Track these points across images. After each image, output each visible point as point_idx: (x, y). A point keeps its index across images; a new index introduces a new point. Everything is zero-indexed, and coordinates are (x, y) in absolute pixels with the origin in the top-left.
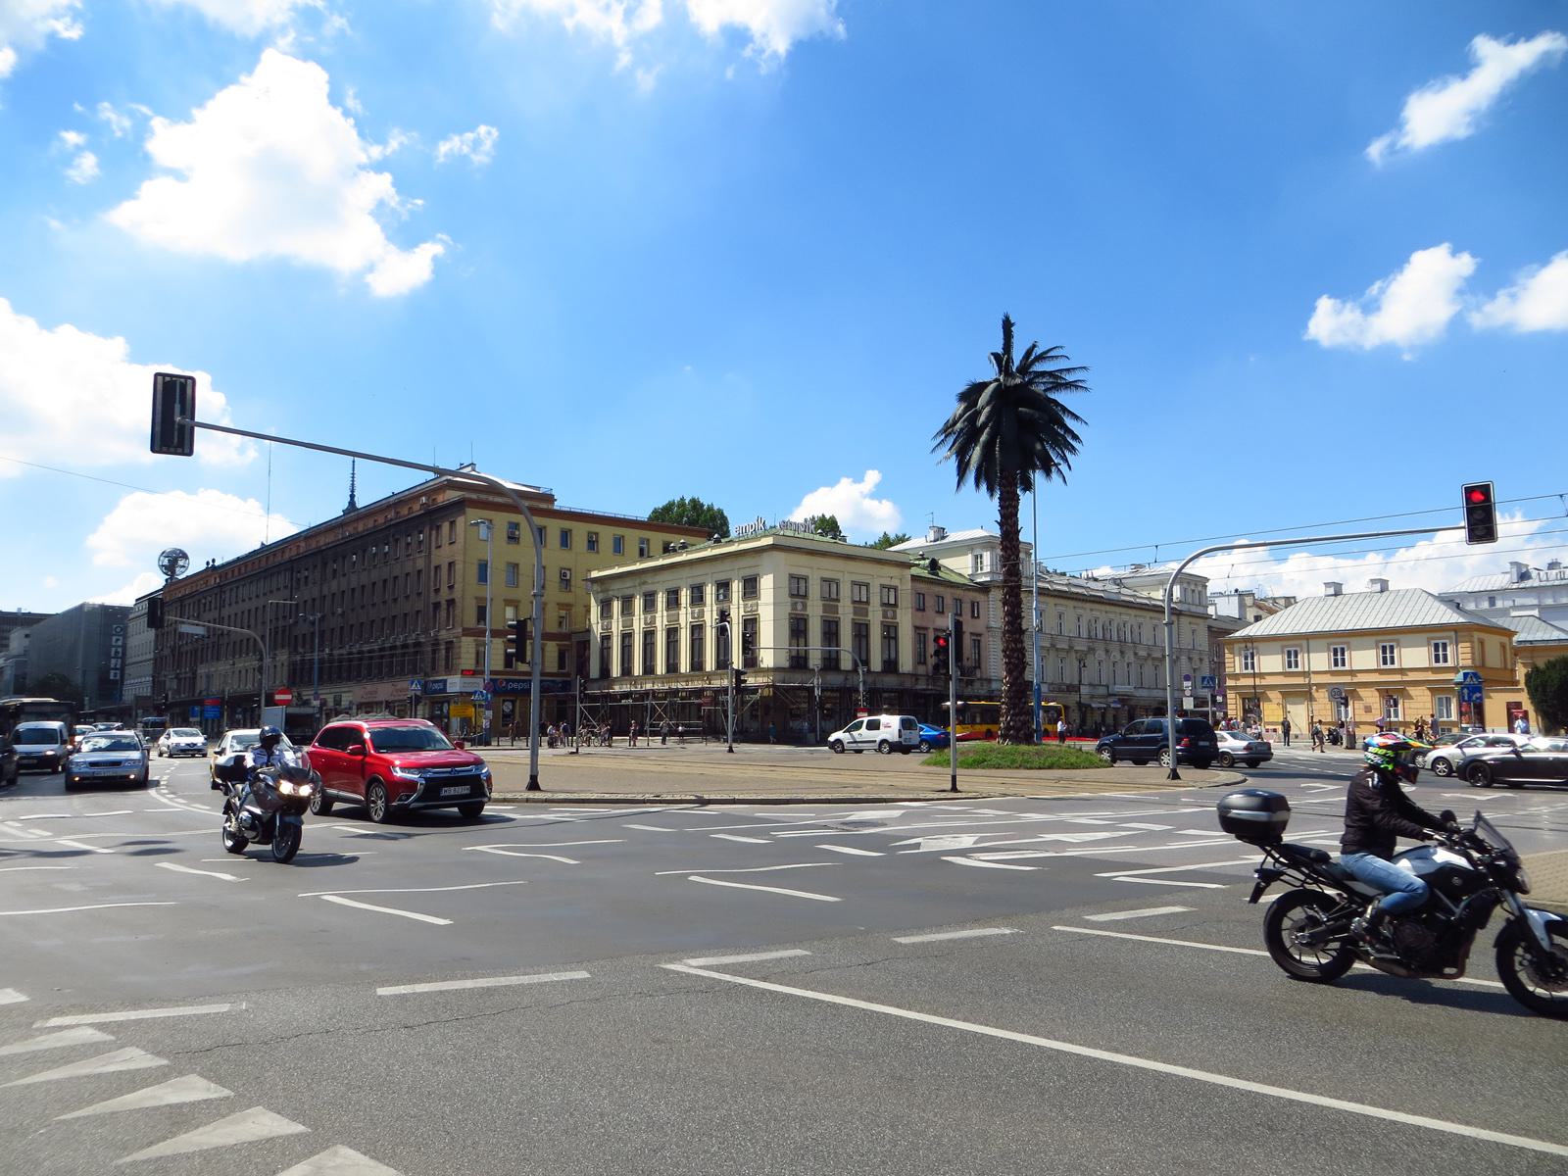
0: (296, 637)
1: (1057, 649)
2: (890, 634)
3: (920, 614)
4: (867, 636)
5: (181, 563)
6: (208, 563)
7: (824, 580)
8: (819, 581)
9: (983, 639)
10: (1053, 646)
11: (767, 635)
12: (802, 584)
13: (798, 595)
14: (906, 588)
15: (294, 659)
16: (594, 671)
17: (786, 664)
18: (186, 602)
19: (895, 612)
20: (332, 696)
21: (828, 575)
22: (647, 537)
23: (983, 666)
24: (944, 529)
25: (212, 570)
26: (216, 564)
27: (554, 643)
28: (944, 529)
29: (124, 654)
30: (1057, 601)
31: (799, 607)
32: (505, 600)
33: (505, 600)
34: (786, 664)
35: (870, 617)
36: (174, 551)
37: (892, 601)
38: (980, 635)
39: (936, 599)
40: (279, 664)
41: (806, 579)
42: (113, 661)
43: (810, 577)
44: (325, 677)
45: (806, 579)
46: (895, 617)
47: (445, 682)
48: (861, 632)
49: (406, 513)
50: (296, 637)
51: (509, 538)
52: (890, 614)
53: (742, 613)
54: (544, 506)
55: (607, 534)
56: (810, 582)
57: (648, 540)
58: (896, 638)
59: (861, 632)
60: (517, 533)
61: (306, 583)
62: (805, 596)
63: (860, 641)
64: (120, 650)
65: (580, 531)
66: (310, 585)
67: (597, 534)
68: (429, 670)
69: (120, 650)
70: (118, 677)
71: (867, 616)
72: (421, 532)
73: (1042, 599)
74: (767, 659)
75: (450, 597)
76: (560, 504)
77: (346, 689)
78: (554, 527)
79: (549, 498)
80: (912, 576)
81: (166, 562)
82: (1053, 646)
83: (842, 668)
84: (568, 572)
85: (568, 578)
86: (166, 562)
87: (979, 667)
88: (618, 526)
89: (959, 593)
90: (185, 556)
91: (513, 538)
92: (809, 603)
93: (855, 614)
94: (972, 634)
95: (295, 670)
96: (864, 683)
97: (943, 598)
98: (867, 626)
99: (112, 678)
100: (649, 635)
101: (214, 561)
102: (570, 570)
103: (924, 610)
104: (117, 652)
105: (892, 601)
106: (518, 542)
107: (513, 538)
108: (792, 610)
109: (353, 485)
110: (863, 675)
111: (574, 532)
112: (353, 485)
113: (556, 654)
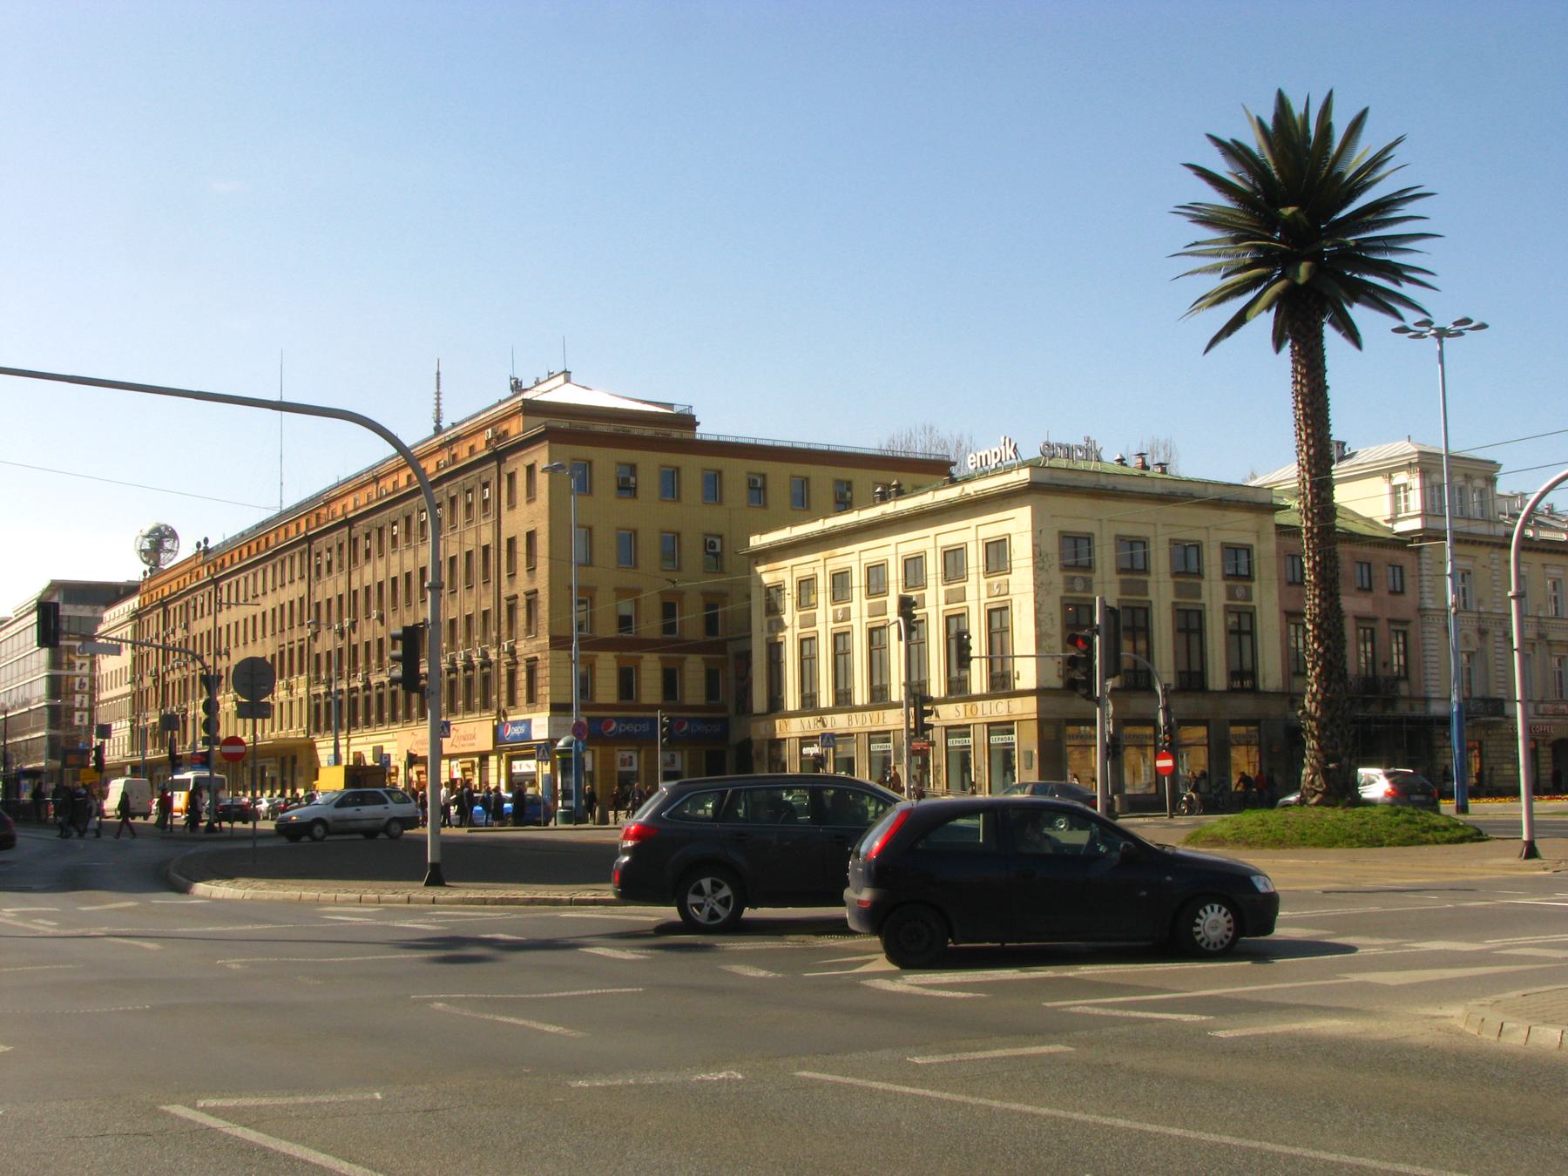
0: (318, 656)
1: (1549, 643)
2: (1242, 628)
3: (1294, 590)
4: (1201, 631)
5: (168, 545)
6: (199, 545)
7: (1120, 539)
8: (1112, 541)
9: (1411, 629)
10: (1541, 636)
11: (1024, 636)
12: (1083, 547)
13: (1076, 567)
14: (1266, 550)
15: (313, 691)
16: (759, 701)
17: (1057, 683)
18: (171, 607)
19: (1248, 591)
20: (370, 747)
21: (1127, 530)
22: (763, 471)
23: (1413, 675)
24: (1344, 444)
25: (205, 552)
26: (210, 545)
27: (655, 656)
28: (1344, 444)
29: (92, 688)
30: (1547, 558)
31: (1079, 585)
32: (616, 590)
33: (616, 590)
34: (1057, 683)
35: (1205, 599)
36: (157, 529)
37: (1366, 585)
38: (1406, 622)
39: (1358, 567)
40: (295, 698)
41: (1144, 543)
42: (78, 698)
43: (1097, 535)
44: (386, 715)
45: (1144, 543)
46: (1248, 597)
47: (528, 722)
48: (1190, 624)
49: (466, 453)
50: (318, 656)
51: (620, 488)
52: (1240, 592)
53: (984, 599)
54: (676, 434)
55: (780, 475)
56: (1152, 547)
57: (764, 476)
58: (1252, 633)
59: (1190, 624)
60: (632, 480)
61: (329, 570)
62: (1089, 567)
63: (1188, 641)
64: (86, 680)
65: (736, 471)
66: (335, 574)
67: (764, 476)
68: (504, 705)
69: (86, 680)
70: (86, 722)
71: (1199, 596)
72: (486, 485)
73: (1526, 556)
74: (1026, 674)
75: (532, 588)
76: (708, 429)
77: (390, 737)
78: (692, 468)
79: (688, 421)
80: (1279, 527)
81: (147, 546)
82: (1541, 636)
83: (1211, 687)
84: (718, 542)
85: (718, 549)
86: (147, 546)
87: (1406, 678)
88: (584, 444)
89: (1366, 551)
90: (173, 535)
91: (626, 488)
92: (1096, 577)
93: (1178, 593)
94: (1391, 621)
95: (318, 707)
96: (1166, 709)
97: (1401, 568)
98: (1200, 614)
99: (77, 722)
100: (841, 641)
101: (206, 541)
102: (720, 537)
103: (1370, 589)
104: (82, 684)
105: (1243, 571)
106: (635, 496)
107: (626, 488)
108: (1067, 590)
109: (438, 410)
110: (1165, 696)
111: (726, 475)
112: (438, 410)
113: (702, 675)
